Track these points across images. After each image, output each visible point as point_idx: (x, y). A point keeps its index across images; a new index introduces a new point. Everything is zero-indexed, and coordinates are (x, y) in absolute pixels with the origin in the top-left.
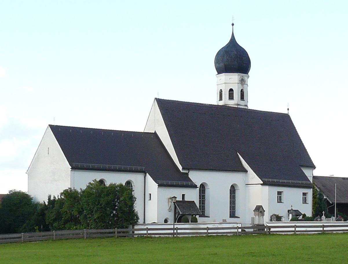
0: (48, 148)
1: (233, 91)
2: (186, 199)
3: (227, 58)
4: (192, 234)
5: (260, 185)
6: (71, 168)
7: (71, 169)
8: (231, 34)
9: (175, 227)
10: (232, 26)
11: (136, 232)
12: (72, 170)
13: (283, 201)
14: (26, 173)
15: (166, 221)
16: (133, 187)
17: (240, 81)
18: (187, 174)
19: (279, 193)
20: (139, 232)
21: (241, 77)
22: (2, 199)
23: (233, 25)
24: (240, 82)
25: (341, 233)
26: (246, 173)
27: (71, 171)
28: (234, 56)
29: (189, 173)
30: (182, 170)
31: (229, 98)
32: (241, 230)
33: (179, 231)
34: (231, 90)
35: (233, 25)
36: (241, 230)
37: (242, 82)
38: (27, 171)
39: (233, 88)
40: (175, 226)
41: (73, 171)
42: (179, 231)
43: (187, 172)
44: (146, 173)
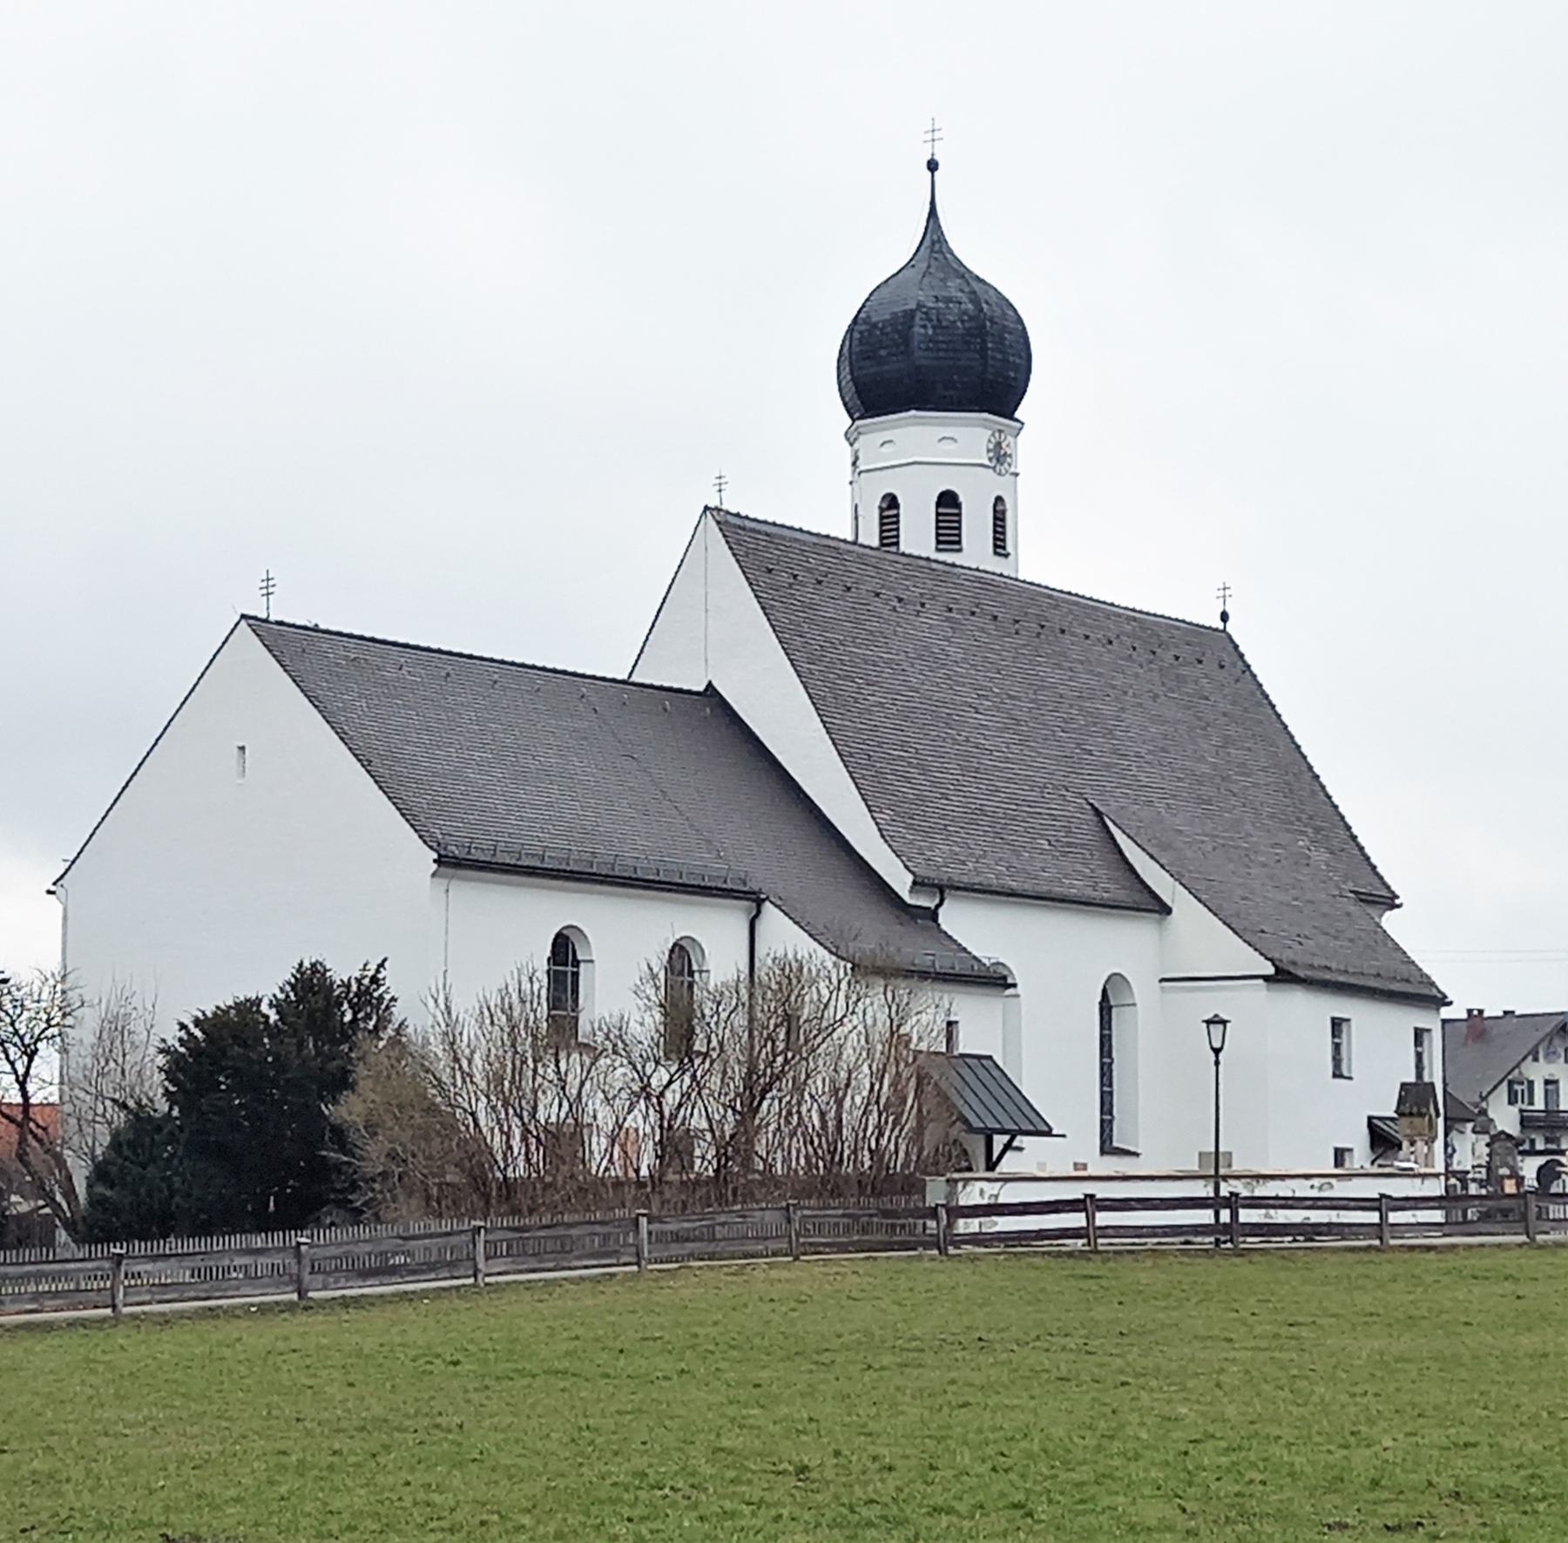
0: (242, 748)
1: (958, 506)
2: (963, 1047)
3: (930, 332)
4: (1133, 1232)
5: (1261, 981)
6: (435, 861)
7: (435, 866)
8: (926, 215)
9: (1224, 1192)
10: (929, 174)
11: (1248, 1216)
12: (442, 869)
13: (1350, 1070)
14: (49, 892)
15: (1340, 1155)
16: (697, 975)
17: (991, 454)
18: (933, 915)
19: (1337, 1025)
20: (1266, 1216)
21: (993, 435)
22: (197, 1022)
23: (932, 166)
24: (990, 459)
25: (909, 1257)
26: (1160, 922)
27: (434, 875)
28: (963, 322)
29: (941, 911)
30: (911, 892)
31: (939, 542)
32: (1228, 1220)
33: (1101, 1219)
34: (948, 500)
35: (932, 166)
36: (1228, 1220)
37: (1000, 457)
38: (55, 884)
39: (943, 488)
40: (1223, 1185)
41: (443, 876)
42: (1247, 1216)
43: (932, 906)
44: (759, 903)
